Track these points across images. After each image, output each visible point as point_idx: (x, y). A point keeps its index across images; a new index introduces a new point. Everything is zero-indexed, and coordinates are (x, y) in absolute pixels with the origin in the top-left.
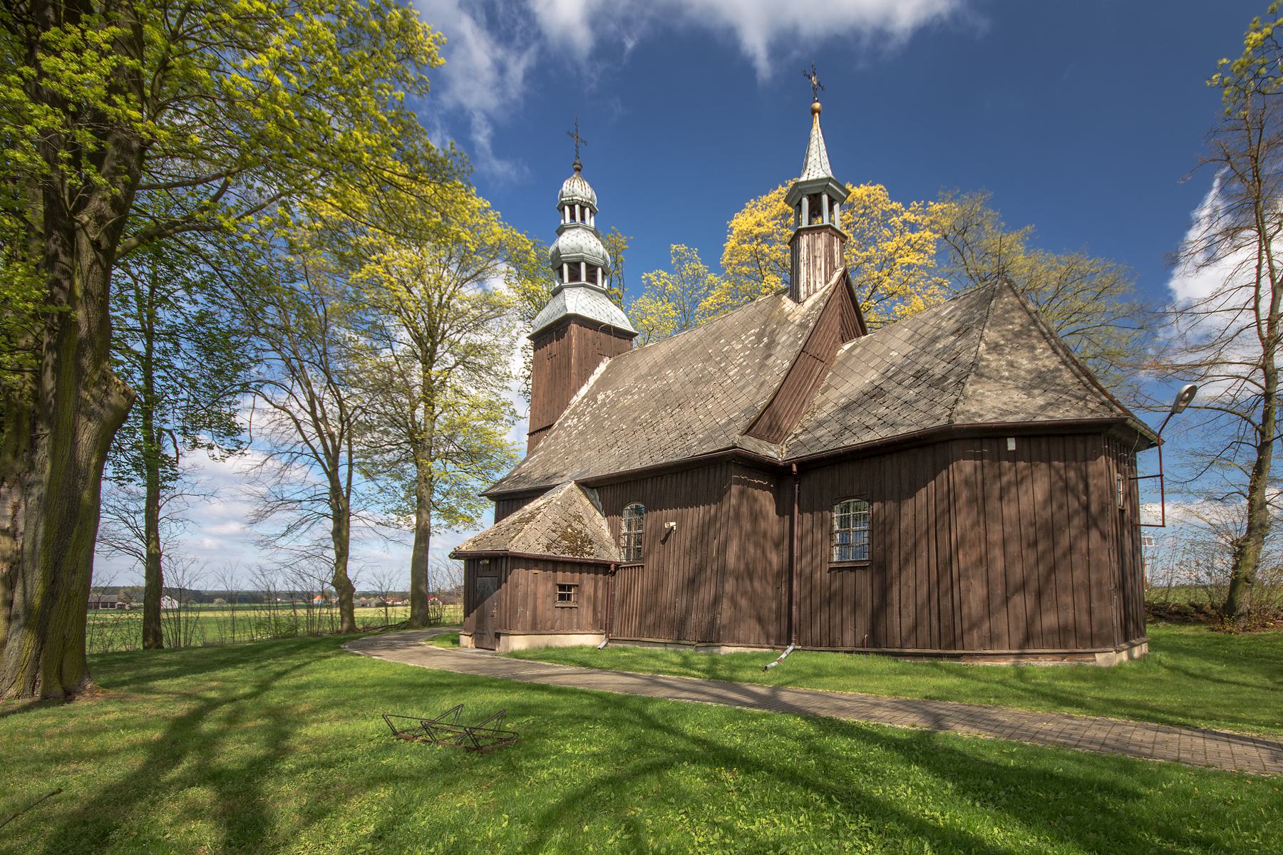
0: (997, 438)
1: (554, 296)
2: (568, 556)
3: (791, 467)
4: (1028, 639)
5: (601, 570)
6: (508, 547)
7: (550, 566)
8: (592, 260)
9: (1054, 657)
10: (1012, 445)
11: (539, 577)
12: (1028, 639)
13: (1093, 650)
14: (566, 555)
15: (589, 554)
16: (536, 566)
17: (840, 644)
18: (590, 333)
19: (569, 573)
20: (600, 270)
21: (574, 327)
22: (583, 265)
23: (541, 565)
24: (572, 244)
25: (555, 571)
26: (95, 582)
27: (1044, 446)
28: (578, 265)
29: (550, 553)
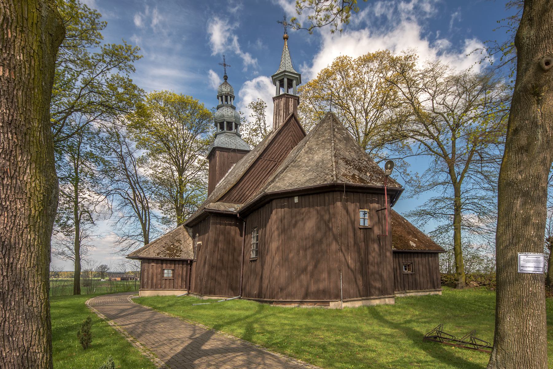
0: (289, 197)
1: (215, 138)
2: (168, 257)
3: (237, 215)
4: (306, 295)
5: (177, 262)
6: (138, 255)
7: (160, 262)
8: (229, 120)
9: (311, 304)
10: (296, 200)
11: (155, 267)
12: (306, 295)
13: (328, 300)
14: (166, 257)
15: (178, 256)
16: (153, 262)
17: (264, 297)
18: (226, 154)
19: (169, 265)
20: (234, 124)
21: (218, 153)
22: (225, 123)
23: (155, 261)
24: (220, 114)
25: (162, 264)
26: (51, 269)
27: (311, 199)
28: (223, 123)
29: (159, 257)
